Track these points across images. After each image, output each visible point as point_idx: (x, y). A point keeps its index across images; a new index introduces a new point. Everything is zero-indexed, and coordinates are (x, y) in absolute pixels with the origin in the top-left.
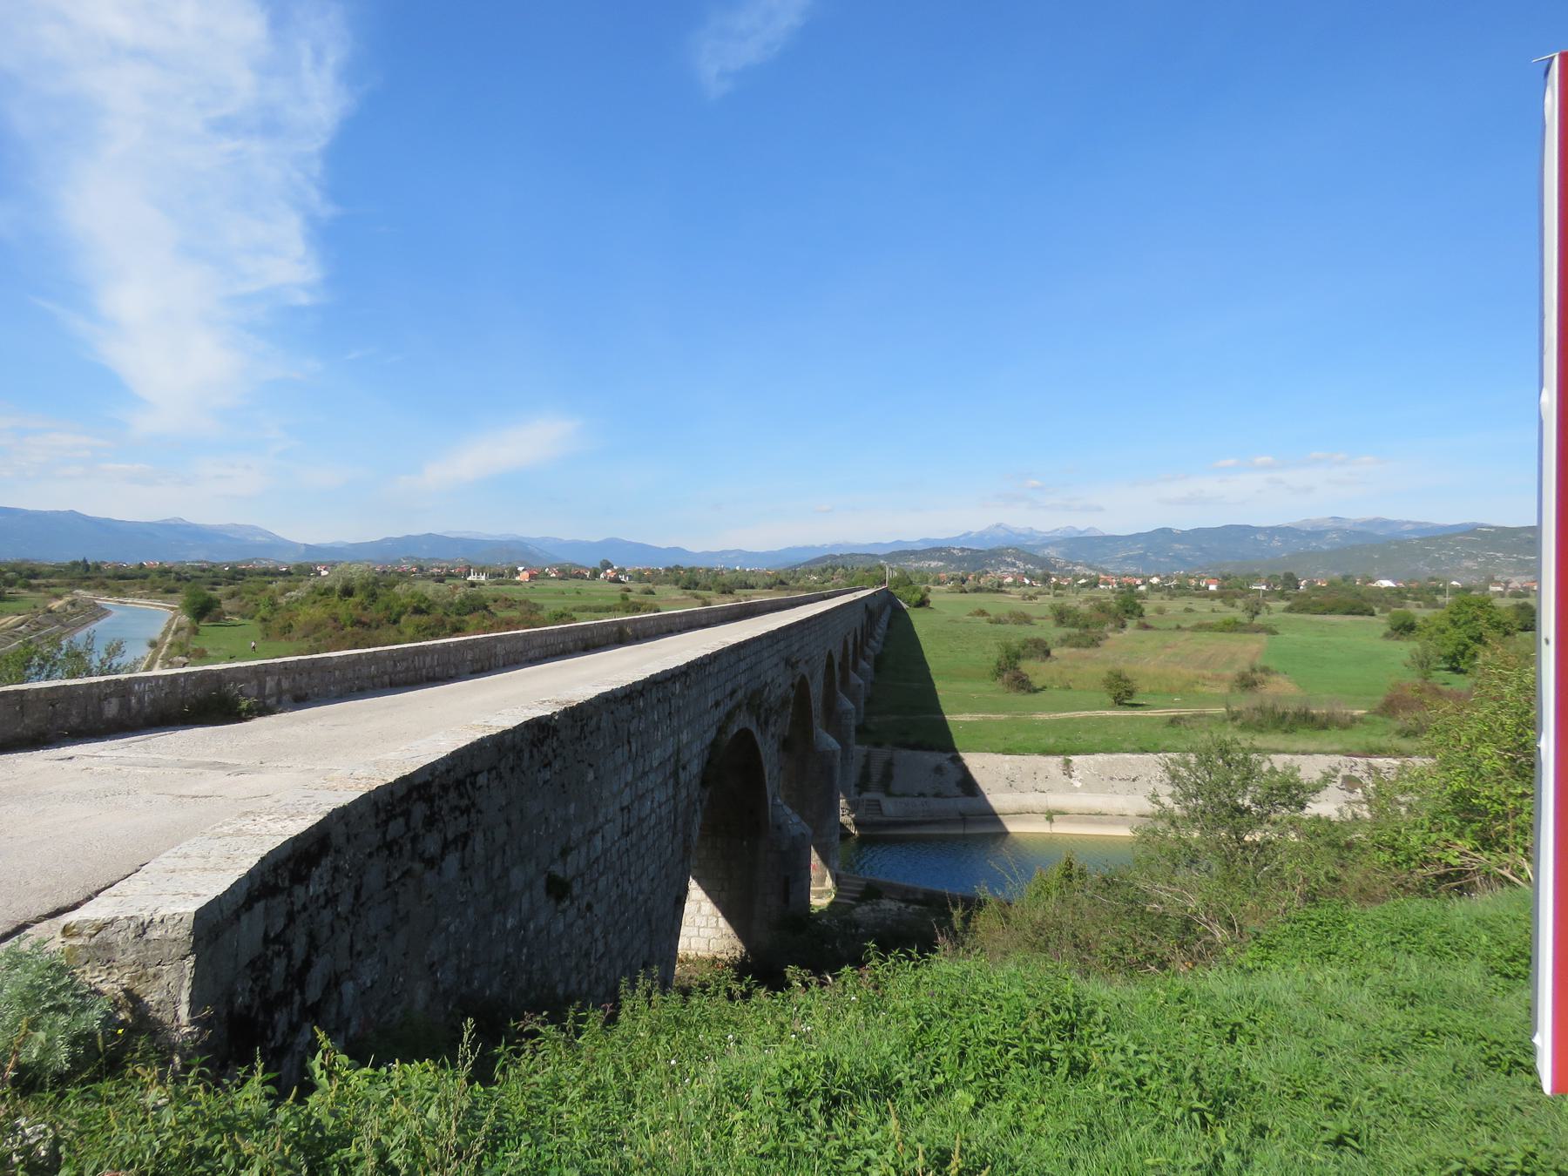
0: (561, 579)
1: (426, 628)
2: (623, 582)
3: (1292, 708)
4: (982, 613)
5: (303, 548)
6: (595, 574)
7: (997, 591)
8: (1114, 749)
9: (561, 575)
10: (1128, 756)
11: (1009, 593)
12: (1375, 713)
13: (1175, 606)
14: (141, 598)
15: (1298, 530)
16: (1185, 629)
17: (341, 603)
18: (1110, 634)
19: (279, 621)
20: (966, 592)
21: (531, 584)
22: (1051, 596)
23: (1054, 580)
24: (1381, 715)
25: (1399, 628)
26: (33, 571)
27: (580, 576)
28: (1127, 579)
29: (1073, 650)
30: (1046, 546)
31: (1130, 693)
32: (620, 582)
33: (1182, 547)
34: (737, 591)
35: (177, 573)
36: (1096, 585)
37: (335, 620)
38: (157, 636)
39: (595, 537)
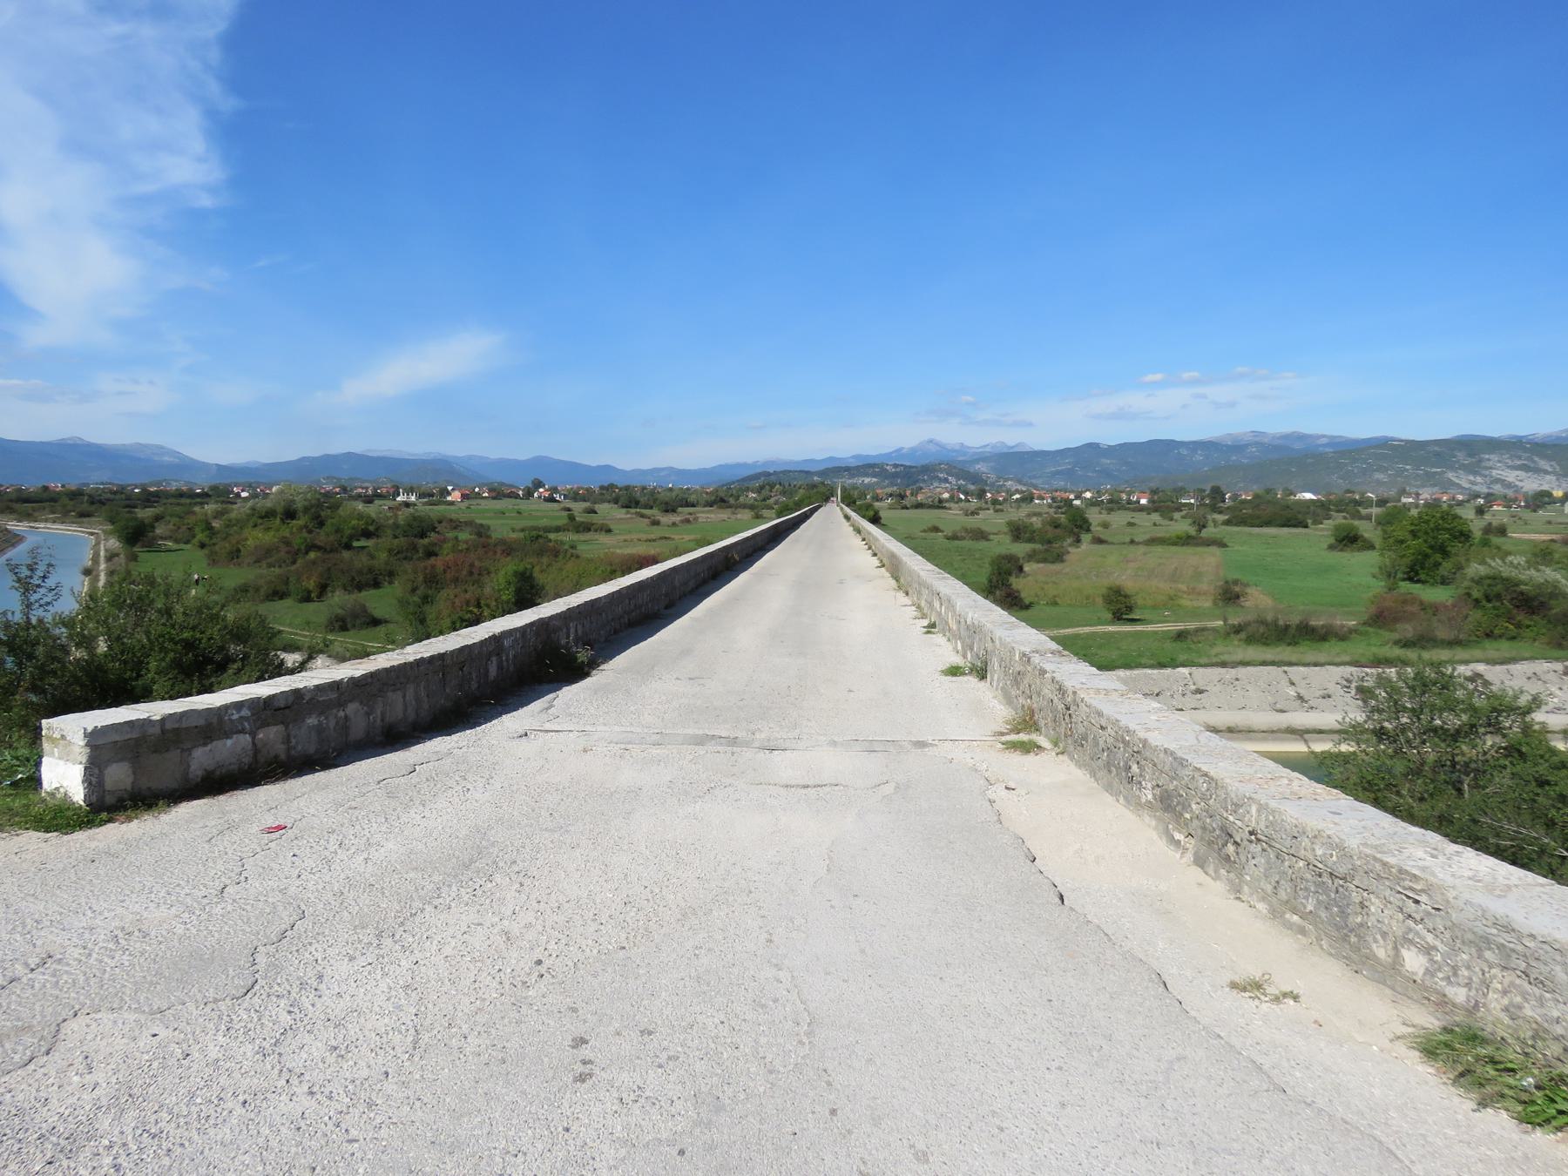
0: (494, 498)
1: (398, 553)
2: (558, 501)
3: (1295, 620)
4: (936, 529)
6: (529, 494)
7: (938, 507)
8: (1133, 665)
9: (494, 494)
10: (1149, 671)
11: (950, 509)
12: (1364, 624)
13: (1119, 519)
14: (54, 522)
15: (1217, 444)
16: (1138, 543)
17: (283, 527)
18: (1070, 549)
19: (223, 547)
20: (907, 508)
22: (991, 511)
23: (989, 495)
24: (1370, 625)
25: (1343, 540)
28: (1058, 493)
29: (1041, 565)
30: (977, 461)
31: (1130, 609)
32: (555, 501)
33: (1109, 461)
34: (680, 509)
35: (90, 496)
36: (1032, 499)
39: (523, 455)
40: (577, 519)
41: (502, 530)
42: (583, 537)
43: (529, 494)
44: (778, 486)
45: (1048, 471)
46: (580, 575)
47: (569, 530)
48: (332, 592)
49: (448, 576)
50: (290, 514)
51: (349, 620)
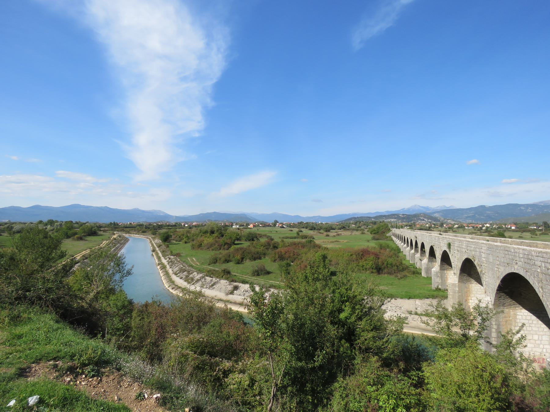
0: (264, 227)
2: (285, 228)
5: (175, 217)
6: (275, 225)
9: (264, 225)
27: (269, 226)
30: (435, 213)
32: (283, 227)
33: (490, 212)
34: (331, 231)
35: (145, 226)
43: (275, 225)
44: (362, 222)
45: (464, 216)
50: (212, 232)
51: (259, 272)
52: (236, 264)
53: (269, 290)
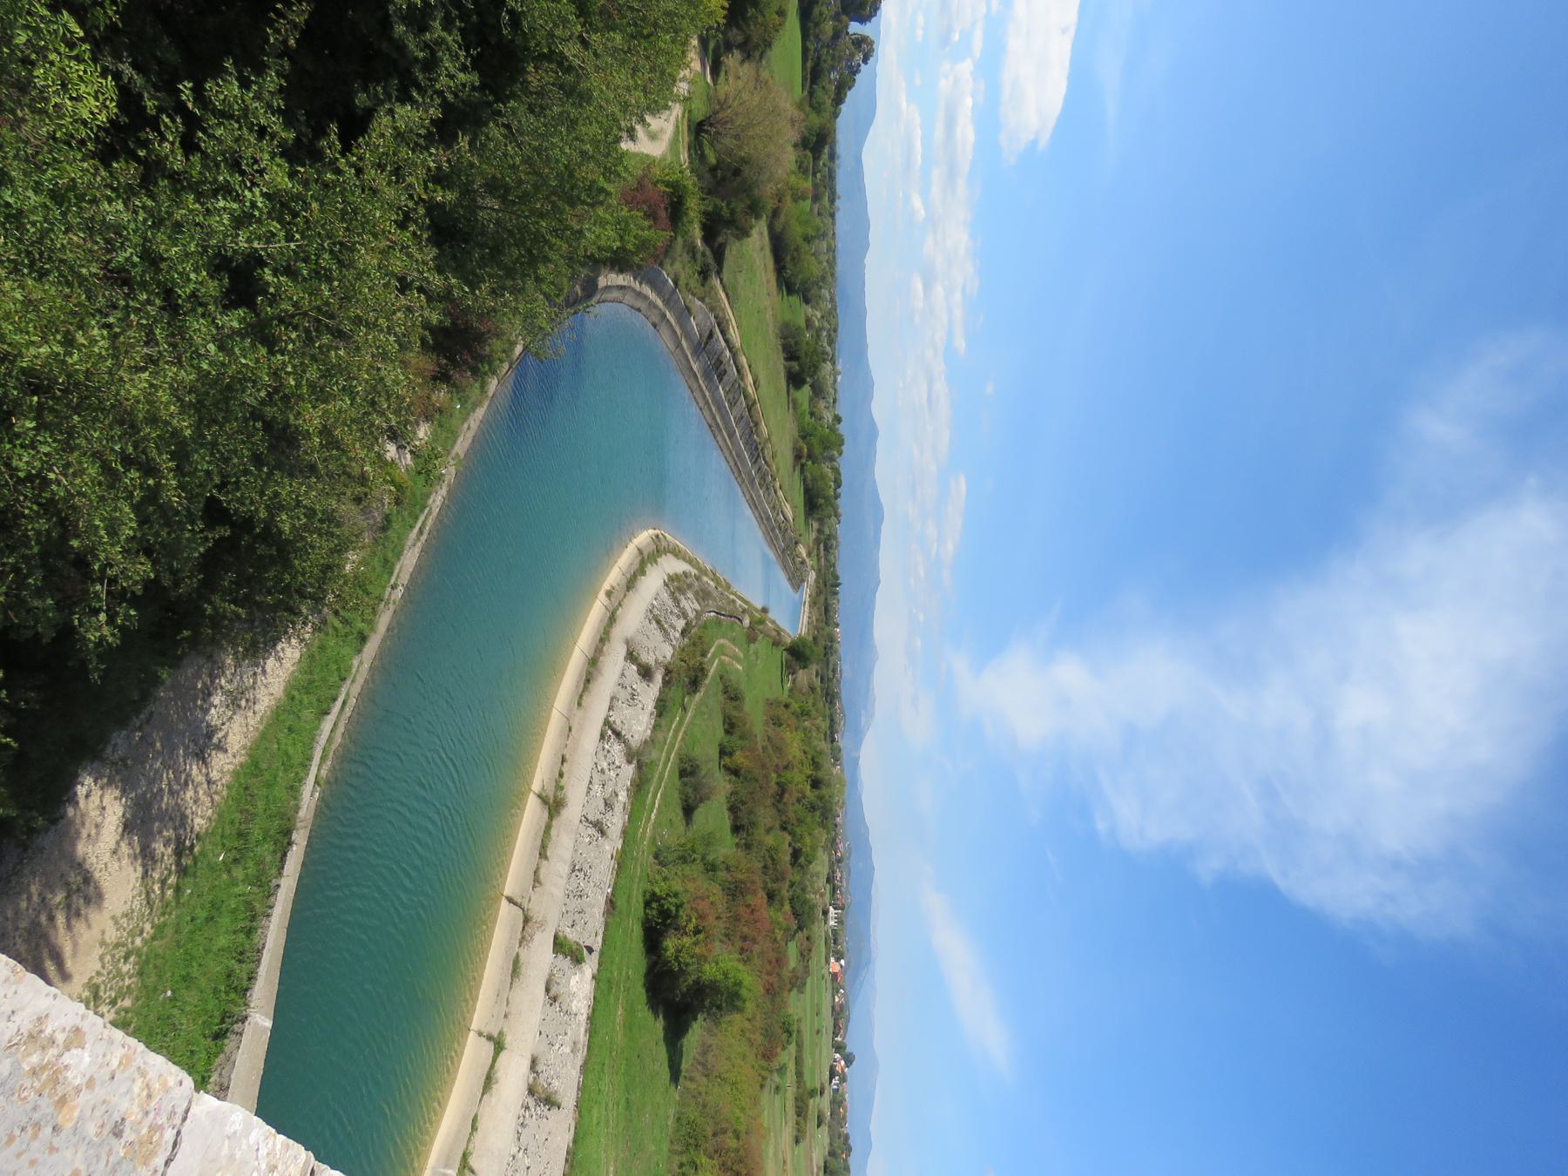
0: (833, 1008)
1: (773, 860)
2: (831, 1082)
6: (839, 1048)
9: (837, 1008)
21: (827, 976)
26: (831, 548)
27: (836, 1030)
32: (831, 1078)
37: (786, 768)
38: (771, 615)
40: (811, 1101)
41: (796, 1006)
42: (790, 1104)
43: (839, 1048)
46: (734, 1084)
47: (798, 1088)
48: (730, 780)
49: (742, 910)
52: (720, 745)
53: (632, 758)
